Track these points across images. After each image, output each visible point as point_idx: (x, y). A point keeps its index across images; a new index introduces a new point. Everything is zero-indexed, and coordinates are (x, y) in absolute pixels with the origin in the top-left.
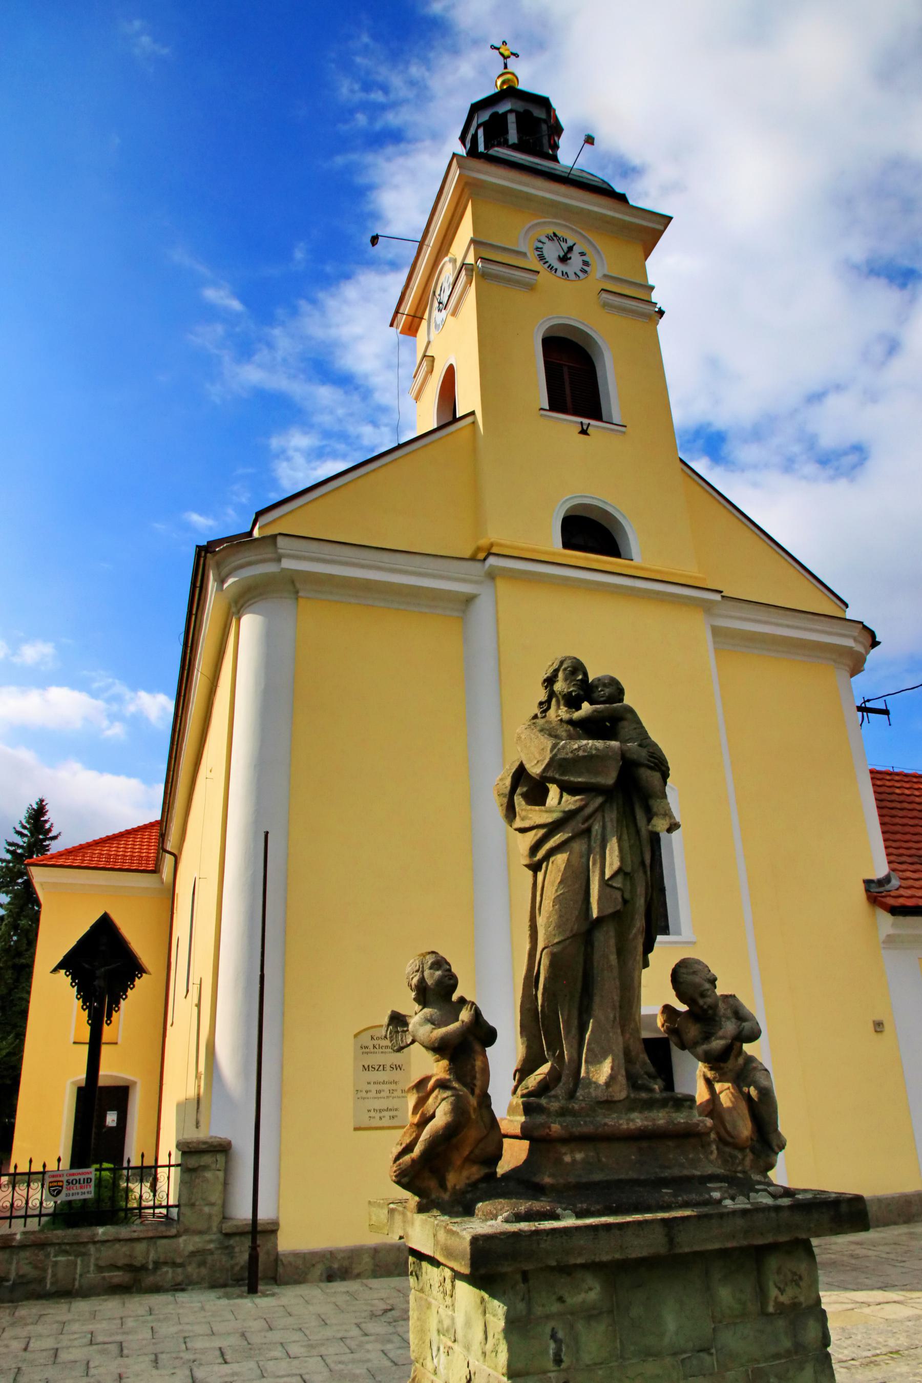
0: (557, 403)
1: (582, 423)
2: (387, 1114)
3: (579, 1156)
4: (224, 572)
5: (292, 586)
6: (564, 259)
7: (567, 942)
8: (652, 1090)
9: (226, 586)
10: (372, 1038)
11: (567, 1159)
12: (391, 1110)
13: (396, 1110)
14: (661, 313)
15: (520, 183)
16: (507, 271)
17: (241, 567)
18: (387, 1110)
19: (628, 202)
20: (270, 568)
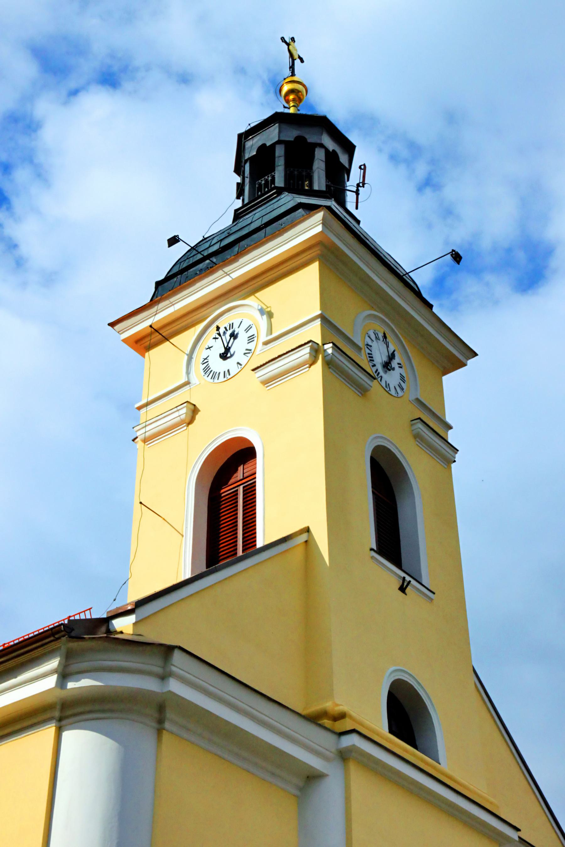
1: (404, 578)
4: (74, 667)
5: (159, 713)
9: (71, 685)
14: (455, 461)
15: (367, 265)
16: (429, 434)
17: (110, 670)
19: (432, 309)
20: (149, 685)
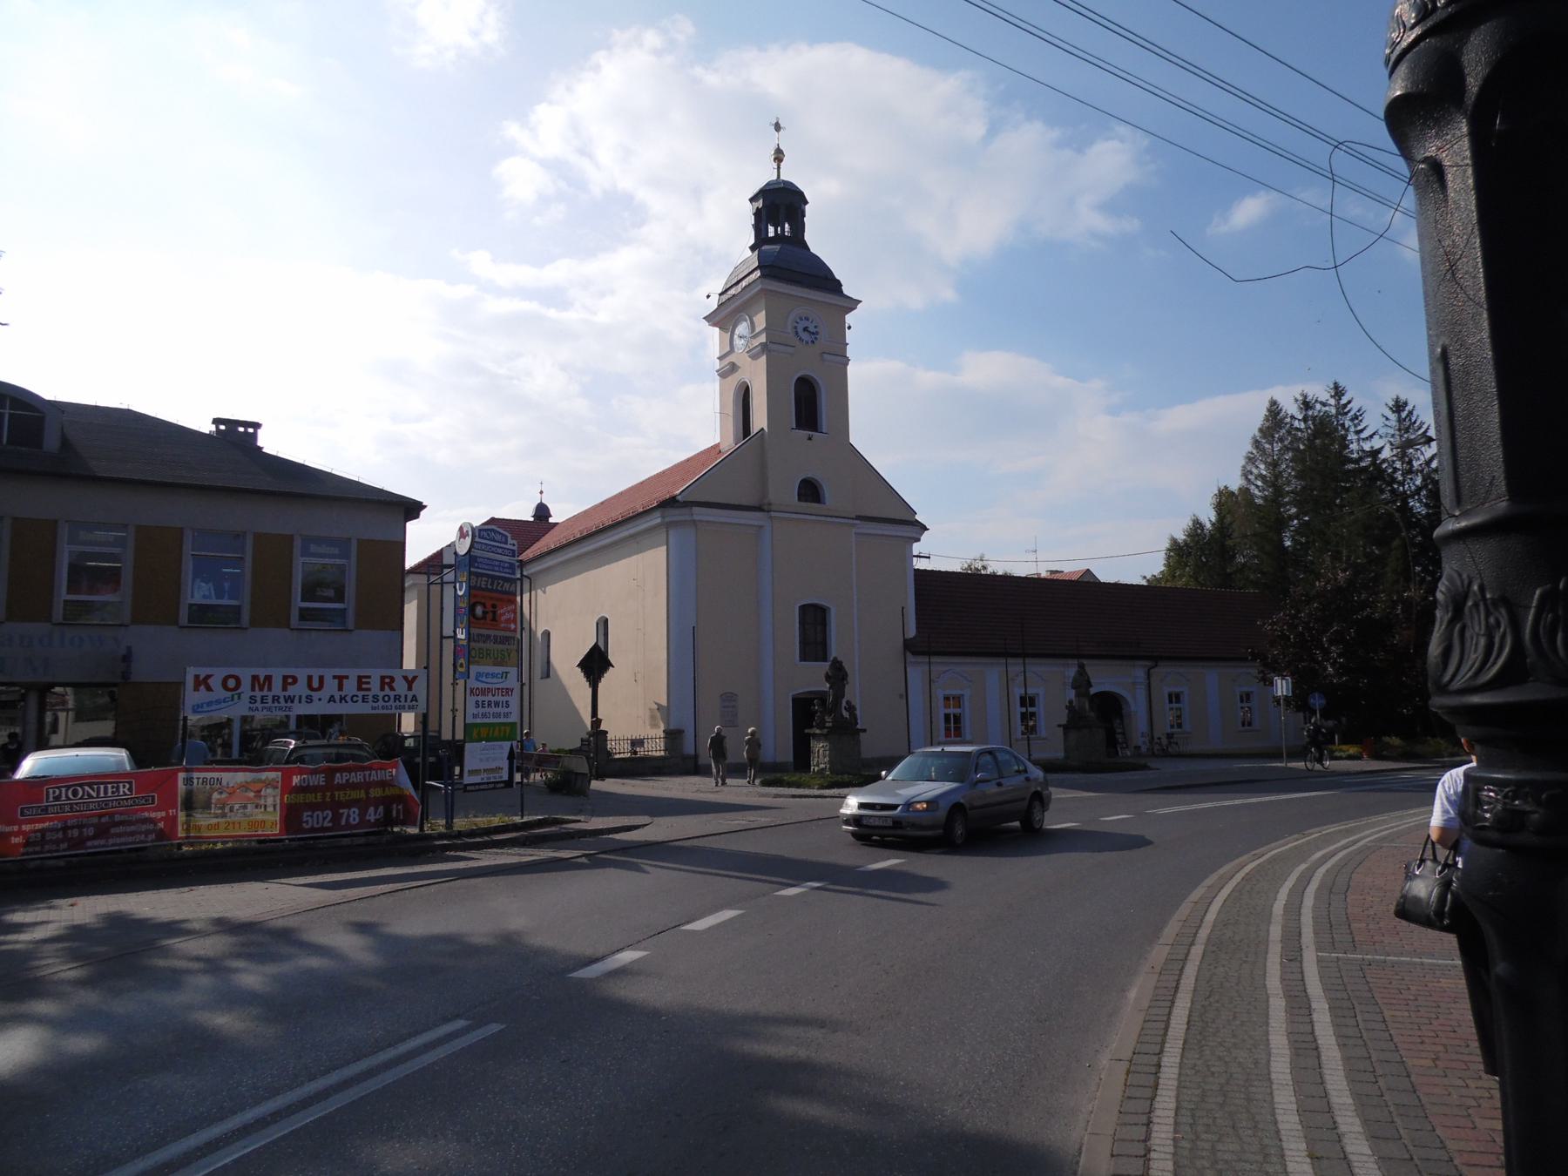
0: (800, 425)
6: (805, 329)
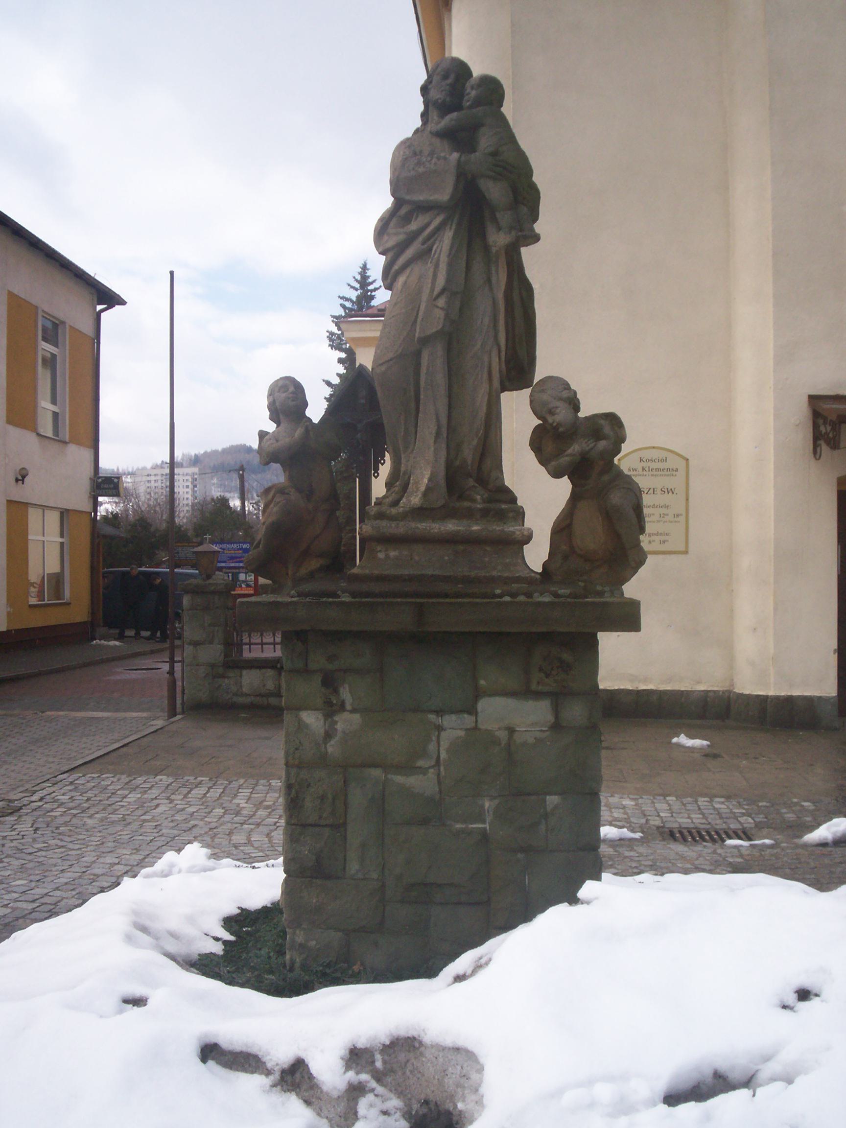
2: (657, 538)
3: (393, 554)
7: (391, 362)
8: (474, 501)
10: (641, 460)
11: (381, 555)
12: (661, 534)
13: (667, 534)
18: (657, 534)
